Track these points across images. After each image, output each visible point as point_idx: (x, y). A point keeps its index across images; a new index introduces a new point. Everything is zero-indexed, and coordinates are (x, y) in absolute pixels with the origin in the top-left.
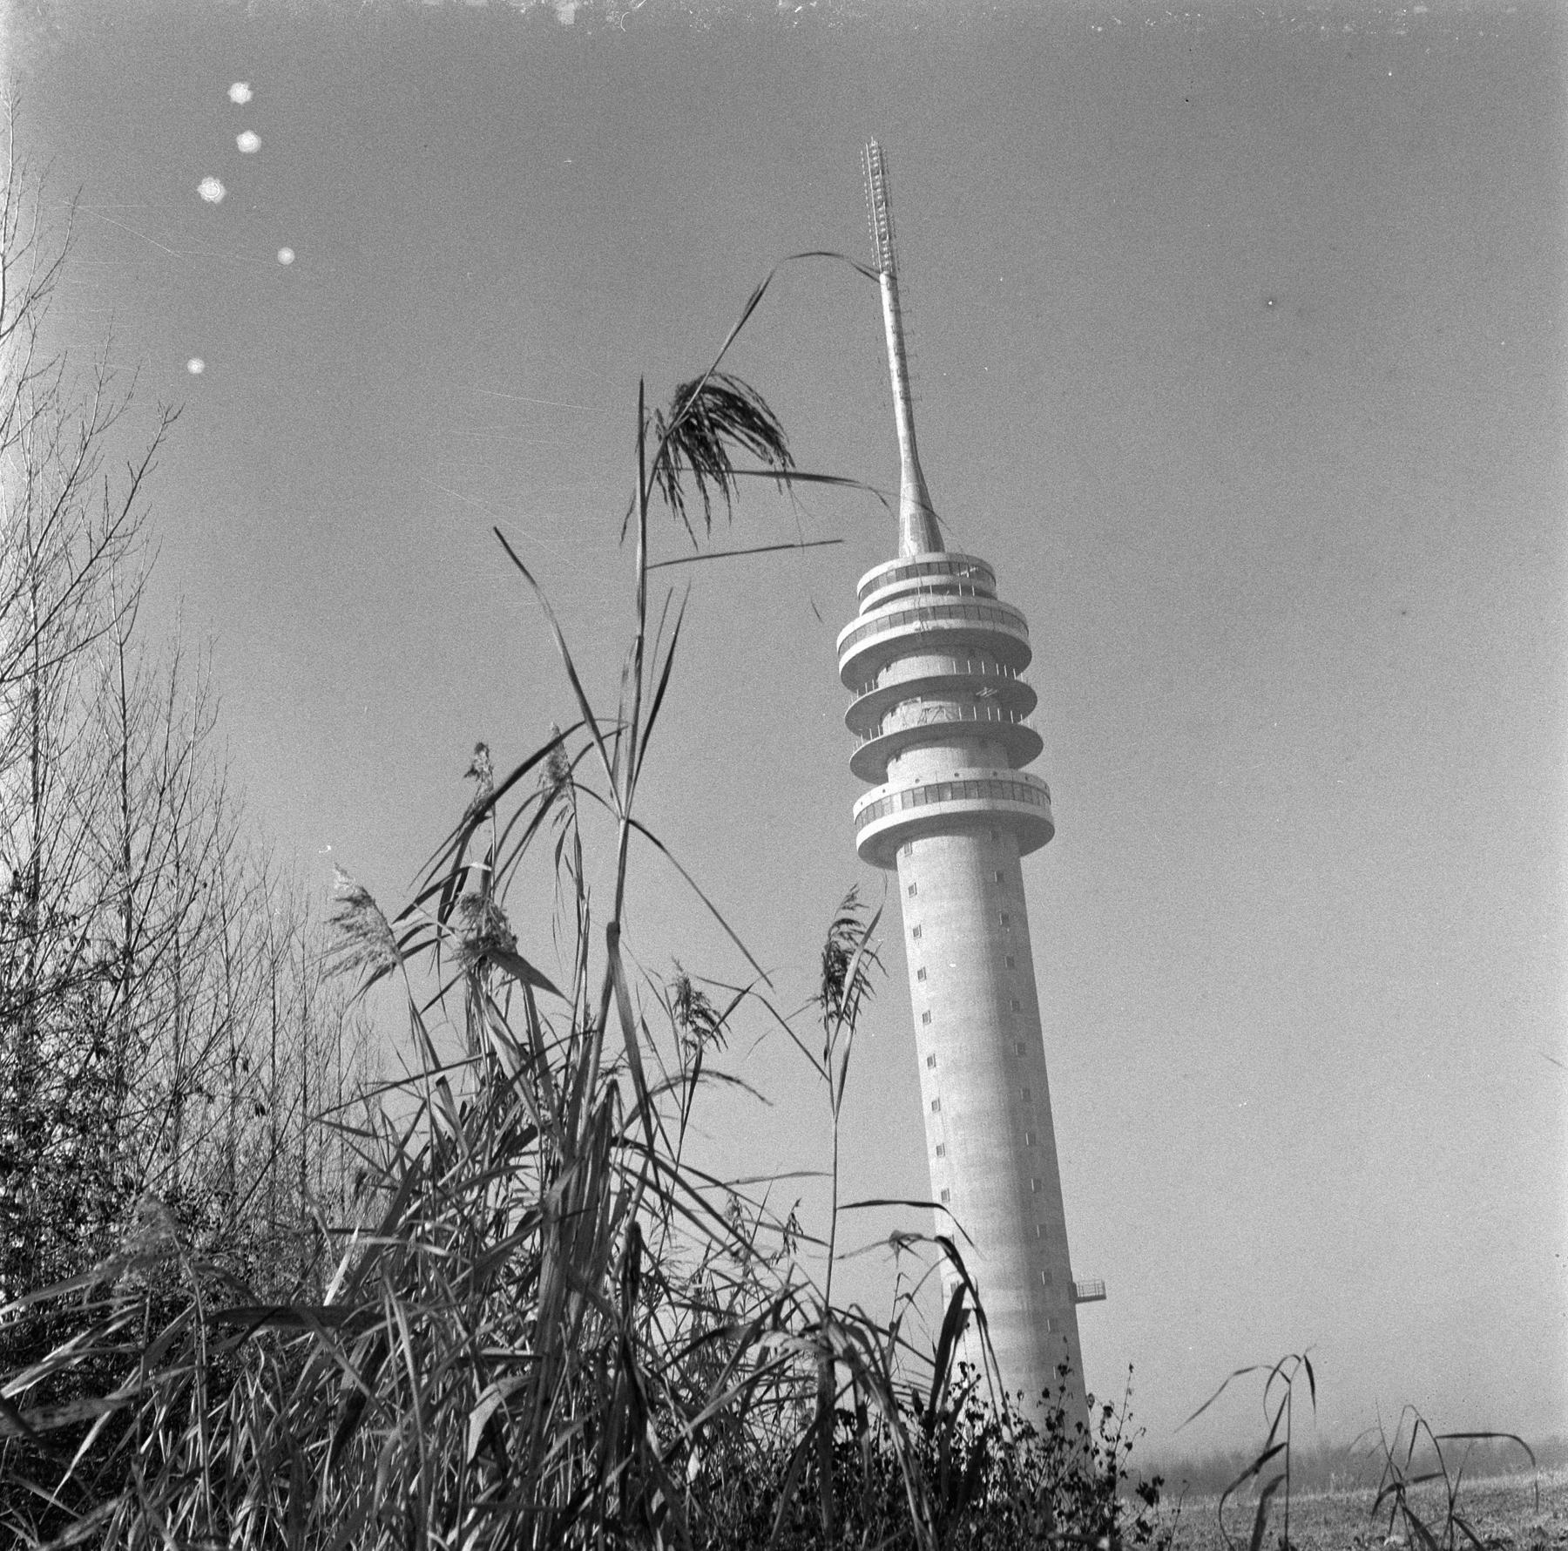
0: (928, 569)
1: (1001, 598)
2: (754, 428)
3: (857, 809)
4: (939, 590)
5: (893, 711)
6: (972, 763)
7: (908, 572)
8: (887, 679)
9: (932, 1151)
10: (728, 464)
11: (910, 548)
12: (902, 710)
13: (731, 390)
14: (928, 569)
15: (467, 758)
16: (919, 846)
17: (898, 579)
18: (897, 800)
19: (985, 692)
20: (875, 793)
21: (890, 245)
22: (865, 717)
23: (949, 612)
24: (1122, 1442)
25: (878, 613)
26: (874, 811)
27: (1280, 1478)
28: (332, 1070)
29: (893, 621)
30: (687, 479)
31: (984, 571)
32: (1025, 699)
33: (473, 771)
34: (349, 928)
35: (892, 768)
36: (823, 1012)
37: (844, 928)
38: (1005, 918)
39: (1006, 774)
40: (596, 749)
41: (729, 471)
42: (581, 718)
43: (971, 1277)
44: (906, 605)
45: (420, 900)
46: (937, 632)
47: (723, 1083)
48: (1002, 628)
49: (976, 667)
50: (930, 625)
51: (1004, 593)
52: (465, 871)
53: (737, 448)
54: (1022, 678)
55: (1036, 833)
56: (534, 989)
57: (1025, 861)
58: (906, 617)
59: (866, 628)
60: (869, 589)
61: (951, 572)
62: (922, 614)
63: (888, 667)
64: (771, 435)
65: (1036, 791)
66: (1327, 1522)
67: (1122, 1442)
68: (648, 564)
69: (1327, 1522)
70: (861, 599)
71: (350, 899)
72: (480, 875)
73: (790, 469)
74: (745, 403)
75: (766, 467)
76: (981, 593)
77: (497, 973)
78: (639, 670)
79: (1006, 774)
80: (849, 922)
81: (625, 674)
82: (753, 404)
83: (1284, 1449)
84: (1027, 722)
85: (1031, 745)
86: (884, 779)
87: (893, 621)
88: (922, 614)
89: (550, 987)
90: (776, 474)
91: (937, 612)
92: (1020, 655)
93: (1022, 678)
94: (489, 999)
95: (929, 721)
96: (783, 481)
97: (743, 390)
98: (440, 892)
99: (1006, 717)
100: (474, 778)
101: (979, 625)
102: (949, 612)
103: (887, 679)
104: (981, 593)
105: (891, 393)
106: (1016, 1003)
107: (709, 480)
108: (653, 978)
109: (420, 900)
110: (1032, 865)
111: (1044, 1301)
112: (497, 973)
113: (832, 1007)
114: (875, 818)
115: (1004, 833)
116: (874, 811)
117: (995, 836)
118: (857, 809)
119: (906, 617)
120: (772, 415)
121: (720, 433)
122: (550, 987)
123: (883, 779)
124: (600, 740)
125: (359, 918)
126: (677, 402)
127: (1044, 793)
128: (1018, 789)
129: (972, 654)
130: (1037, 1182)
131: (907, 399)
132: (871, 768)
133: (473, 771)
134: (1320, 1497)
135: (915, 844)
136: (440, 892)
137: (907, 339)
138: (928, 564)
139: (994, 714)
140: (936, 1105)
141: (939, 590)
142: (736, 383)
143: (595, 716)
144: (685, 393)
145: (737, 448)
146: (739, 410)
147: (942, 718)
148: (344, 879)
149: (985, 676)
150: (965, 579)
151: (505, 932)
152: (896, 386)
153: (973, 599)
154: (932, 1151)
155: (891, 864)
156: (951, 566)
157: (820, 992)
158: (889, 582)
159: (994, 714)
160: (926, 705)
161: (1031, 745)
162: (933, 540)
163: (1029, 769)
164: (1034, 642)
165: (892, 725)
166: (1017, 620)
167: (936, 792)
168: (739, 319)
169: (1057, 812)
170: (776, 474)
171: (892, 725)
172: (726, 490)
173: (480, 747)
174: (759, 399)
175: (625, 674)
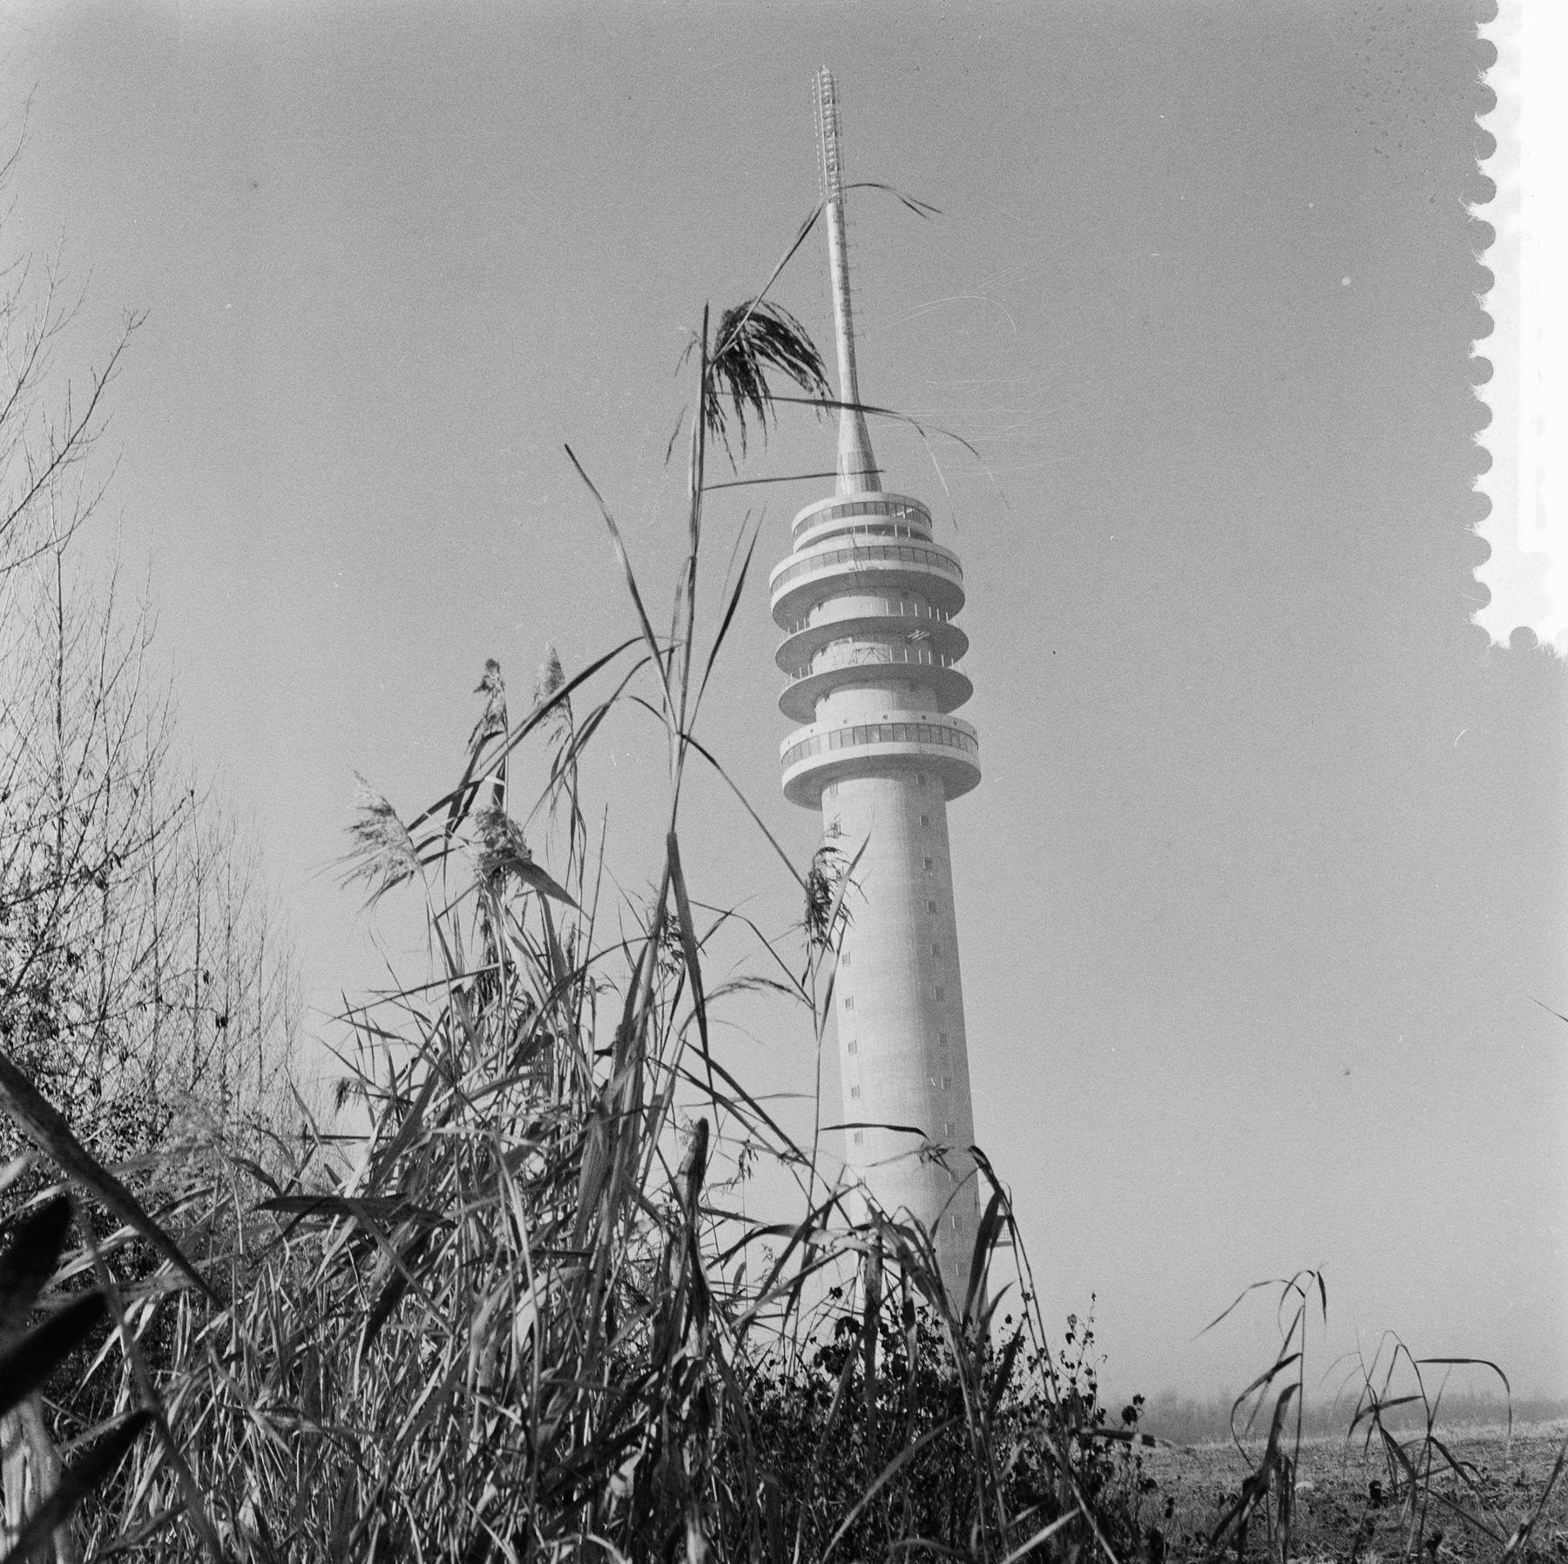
0: (865, 508)
1: (936, 541)
2: (795, 353)
3: (784, 747)
4: (875, 529)
5: (824, 650)
6: (901, 706)
7: (844, 510)
8: (820, 617)
9: (847, 1092)
10: (766, 390)
11: (848, 488)
12: (832, 649)
13: (774, 318)
14: (865, 508)
15: (478, 673)
16: (846, 787)
17: (834, 516)
18: (825, 741)
19: (916, 635)
20: (803, 733)
21: (838, 177)
22: (793, 656)
23: (884, 552)
24: (1083, 1368)
25: (812, 551)
26: (800, 751)
27: (1293, 1388)
28: (253, 993)
29: (827, 559)
30: (726, 402)
31: (921, 513)
32: (956, 644)
33: (484, 686)
34: (369, 836)
35: (821, 707)
36: (808, 938)
37: (828, 855)
38: (928, 862)
39: (934, 718)
40: (654, 660)
41: (767, 396)
42: (640, 632)
43: (1003, 1186)
44: (842, 543)
45: (432, 810)
46: (870, 573)
47: (776, 990)
48: (935, 571)
49: (909, 609)
50: (865, 565)
51: (941, 535)
52: (476, 785)
53: (774, 375)
54: (954, 622)
55: (960, 778)
56: (549, 898)
57: (951, 806)
58: (840, 556)
59: (798, 566)
60: (803, 526)
61: (887, 513)
62: (858, 553)
63: (820, 605)
64: (810, 359)
65: (963, 736)
66: (1232, 1469)
67: (1083, 1368)
68: (705, 485)
69: (1232, 1469)
70: (795, 536)
71: (370, 808)
72: (492, 788)
73: (828, 398)
74: (786, 331)
75: (805, 395)
76: (917, 535)
77: (513, 882)
78: (692, 591)
79: (934, 718)
80: (833, 850)
81: (679, 593)
82: (794, 333)
83: (1298, 1359)
84: (956, 667)
85: (960, 690)
86: (812, 719)
87: (827, 559)
88: (858, 553)
89: (568, 899)
90: (816, 402)
91: (870, 552)
92: (953, 599)
93: (954, 622)
94: (507, 911)
95: (860, 663)
96: (822, 409)
97: (785, 319)
98: (449, 805)
99: (937, 660)
100: (484, 693)
101: (911, 567)
102: (884, 552)
103: (820, 617)
104: (917, 535)
105: (833, 330)
106: (936, 948)
107: (748, 406)
108: (633, 900)
109: (432, 810)
110: (956, 810)
111: (953, 1246)
112: (513, 882)
113: (815, 933)
114: (802, 757)
115: (933, 776)
116: (800, 751)
117: (922, 779)
118: (784, 747)
119: (840, 556)
120: (811, 345)
121: (760, 359)
122: (568, 899)
123: (812, 719)
124: (658, 654)
125: (378, 826)
126: (724, 328)
127: (972, 737)
128: (946, 733)
129: (905, 595)
130: (951, 1127)
131: (850, 335)
132: (799, 707)
133: (484, 686)
134: (1220, 1447)
135: (840, 785)
136: (449, 805)
137: (851, 275)
138: (865, 504)
139: (925, 658)
140: (852, 1047)
141: (875, 529)
142: (778, 311)
143: (655, 633)
144: (732, 319)
145: (774, 375)
146: (781, 339)
147: (873, 660)
148: (364, 788)
149: (919, 618)
150: (905, 522)
151: (521, 845)
152: (839, 320)
153: (908, 541)
154: (847, 1092)
155: (817, 805)
156: (888, 507)
157: (804, 919)
158: (825, 520)
159: (925, 658)
160: (858, 645)
161: (960, 690)
162: (871, 475)
163: (955, 714)
164: (968, 586)
165: (823, 664)
166: (950, 562)
167: (865, 733)
168: (790, 248)
169: (985, 758)
170: (816, 402)
171: (823, 664)
172: (762, 417)
173: (491, 664)
174: (800, 328)
175: (679, 593)
